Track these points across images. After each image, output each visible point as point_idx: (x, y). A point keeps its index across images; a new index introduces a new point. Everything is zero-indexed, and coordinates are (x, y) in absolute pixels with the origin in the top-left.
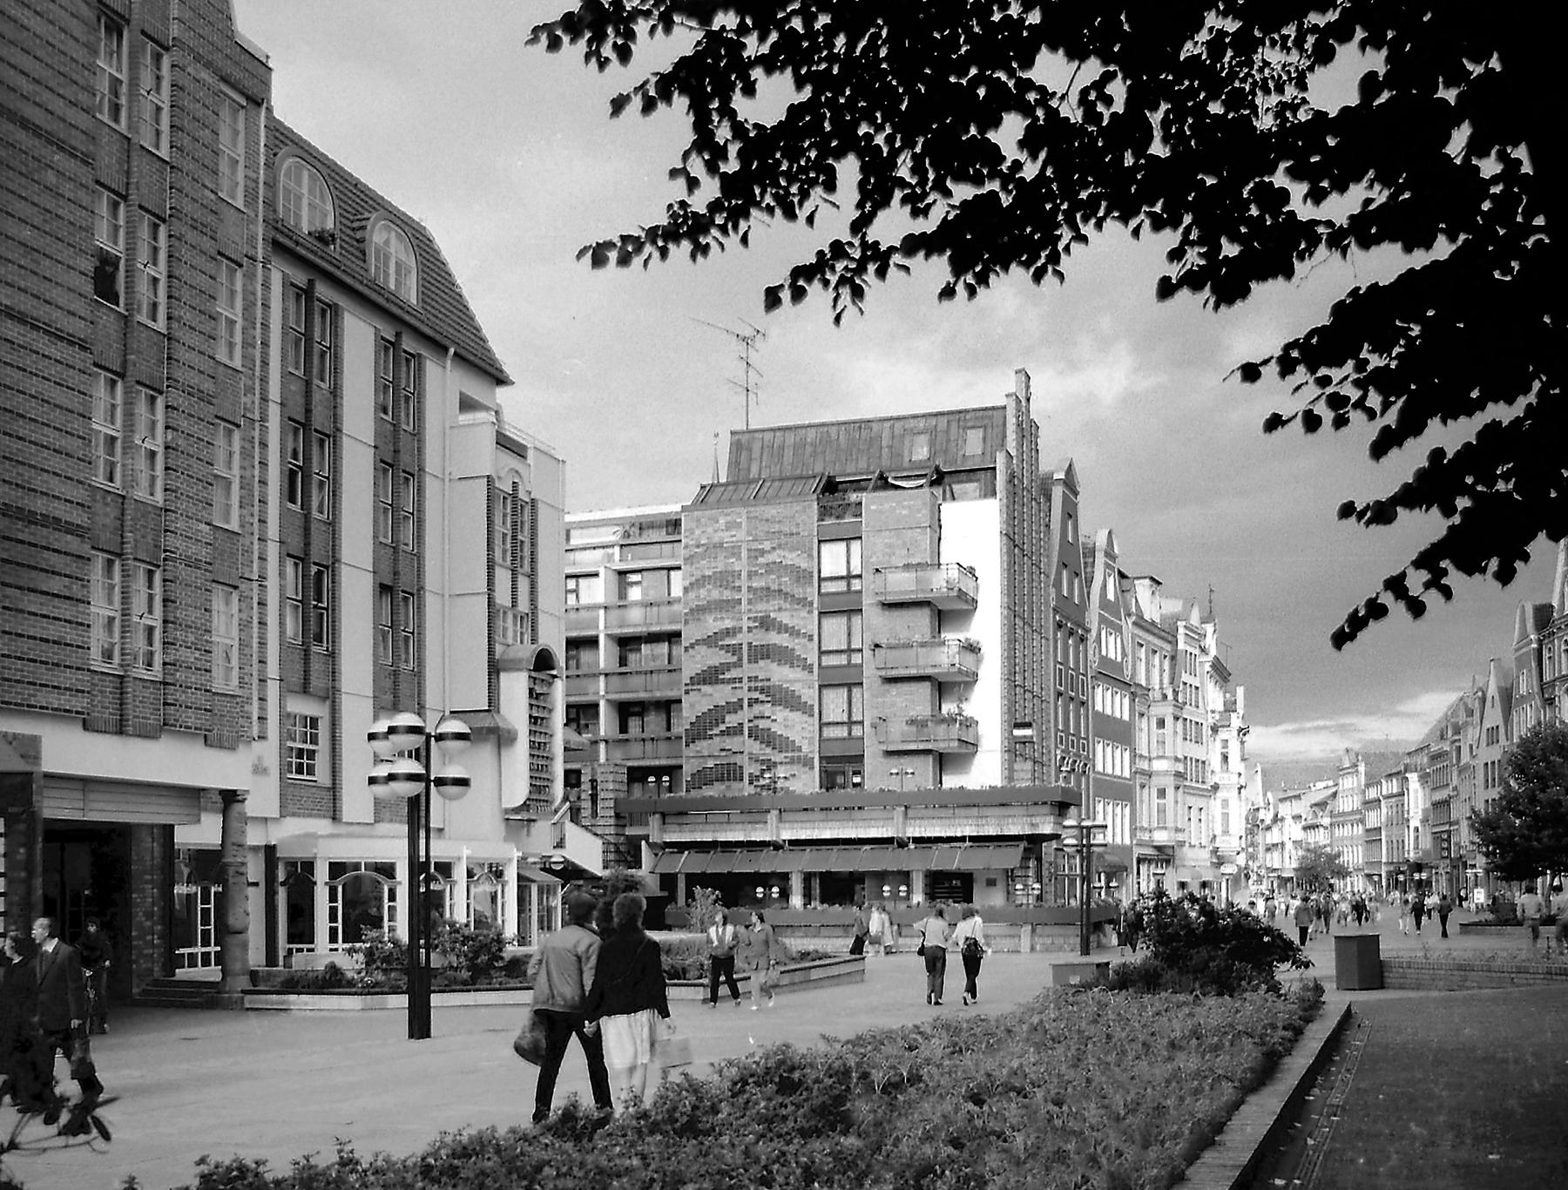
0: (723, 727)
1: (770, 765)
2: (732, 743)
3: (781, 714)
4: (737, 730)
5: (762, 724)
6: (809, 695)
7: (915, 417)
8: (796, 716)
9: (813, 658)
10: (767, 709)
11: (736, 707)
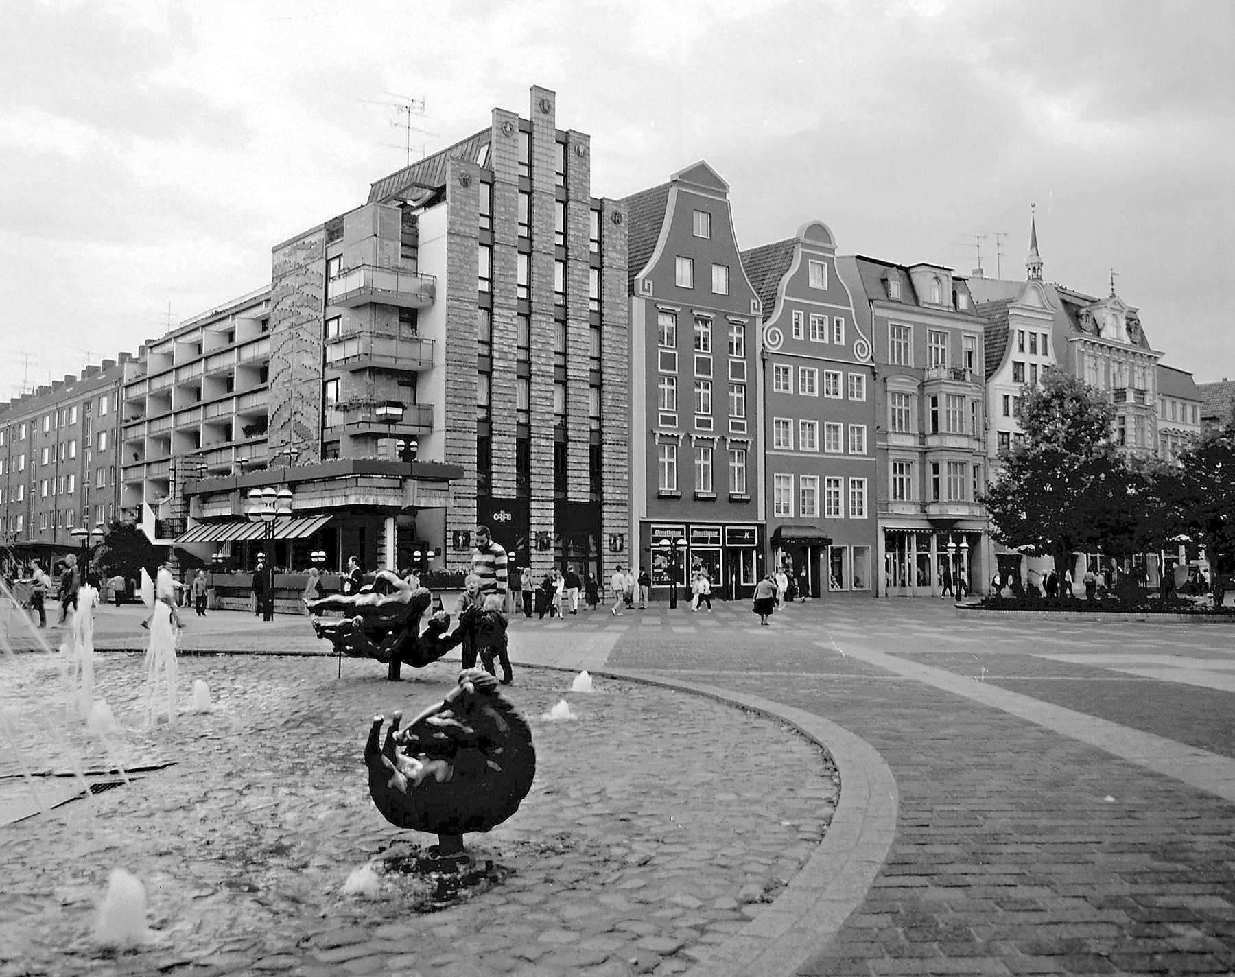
7: (457, 145)
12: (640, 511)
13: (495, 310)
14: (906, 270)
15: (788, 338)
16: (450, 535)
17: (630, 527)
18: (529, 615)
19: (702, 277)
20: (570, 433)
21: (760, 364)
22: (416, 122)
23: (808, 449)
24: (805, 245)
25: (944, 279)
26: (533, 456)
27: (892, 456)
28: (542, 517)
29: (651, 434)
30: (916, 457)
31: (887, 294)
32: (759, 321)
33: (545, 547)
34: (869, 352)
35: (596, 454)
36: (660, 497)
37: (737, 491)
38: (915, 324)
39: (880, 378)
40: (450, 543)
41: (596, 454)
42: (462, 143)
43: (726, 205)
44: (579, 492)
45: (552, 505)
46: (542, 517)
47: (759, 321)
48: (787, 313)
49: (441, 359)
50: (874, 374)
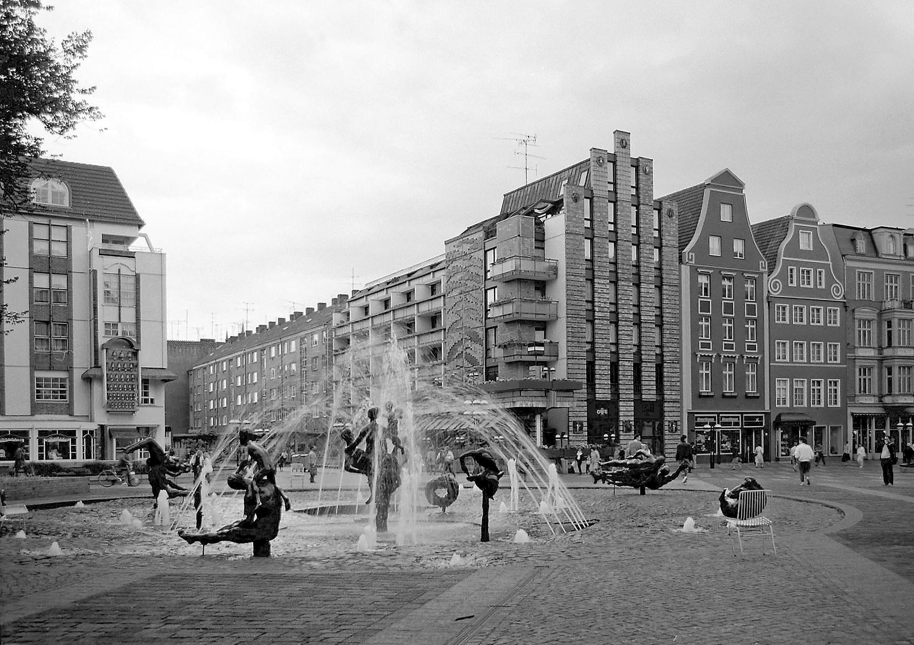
2: (459, 362)
5: (468, 351)
7: (565, 170)
8: (478, 346)
11: (460, 342)
12: (688, 404)
13: (596, 280)
14: (869, 232)
15: (785, 286)
16: (571, 424)
17: (681, 416)
19: (726, 247)
20: (643, 357)
21: (766, 305)
22: (531, 149)
23: (799, 360)
24: (797, 221)
25: (897, 236)
26: (620, 373)
27: (858, 363)
28: (627, 411)
29: (694, 355)
30: (875, 363)
31: (855, 249)
32: (765, 276)
33: (629, 430)
34: (842, 292)
35: (659, 368)
36: (700, 396)
37: (751, 390)
38: (875, 270)
39: (849, 309)
40: (571, 429)
41: (659, 368)
42: (569, 169)
43: (743, 197)
44: (649, 395)
45: (632, 403)
46: (627, 411)
47: (765, 276)
48: (784, 268)
49: (563, 313)
50: (846, 307)
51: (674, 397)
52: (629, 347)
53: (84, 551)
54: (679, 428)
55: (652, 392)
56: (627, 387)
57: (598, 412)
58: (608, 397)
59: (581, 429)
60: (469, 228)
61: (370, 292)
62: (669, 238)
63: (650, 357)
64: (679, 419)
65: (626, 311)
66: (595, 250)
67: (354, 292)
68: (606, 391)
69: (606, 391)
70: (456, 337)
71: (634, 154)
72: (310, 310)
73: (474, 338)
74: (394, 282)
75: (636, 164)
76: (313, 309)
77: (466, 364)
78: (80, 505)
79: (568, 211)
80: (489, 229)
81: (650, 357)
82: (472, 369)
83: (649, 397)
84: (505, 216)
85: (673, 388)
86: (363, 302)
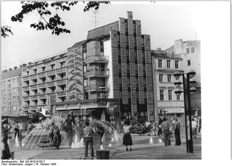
0: (73, 88)
1: (78, 95)
2: (74, 91)
3: (79, 85)
4: (74, 89)
5: (77, 87)
6: (82, 81)
8: (81, 86)
9: (82, 74)
10: (77, 85)
11: (74, 85)
18: (200, 64)
45: (136, 105)
51: (151, 103)
52: (134, 85)
53: (51, 147)
54: (153, 113)
55: (143, 101)
56: (135, 99)
57: (124, 108)
58: (128, 103)
59: (118, 115)
60: (76, 44)
61: (36, 64)
62: (147, 47)
63: (142, 89)
64: (153, 110)
65: (133, 73)
66: (106, 26)
67: (30, 63)
68: (127, 101)
69: (127, 101)
70: (72, 82)
71: (134, 19)
72: (11, 69)
73: (79, 83)
74: (45, 62)
75: (134, 22)
76: (12, 69)
77: (76, 92)
78: (108, 135)
79: (112, 40)
80: (84, 44)
81: (142, 89)
82: (79, 94)
83: (142, 103)
84: (89, 41)
85: (150, 99)
86: (35, 68)
